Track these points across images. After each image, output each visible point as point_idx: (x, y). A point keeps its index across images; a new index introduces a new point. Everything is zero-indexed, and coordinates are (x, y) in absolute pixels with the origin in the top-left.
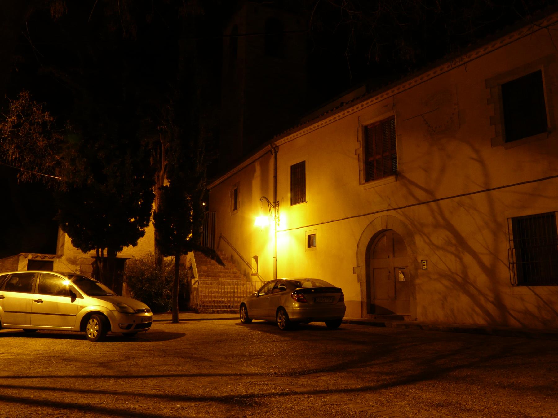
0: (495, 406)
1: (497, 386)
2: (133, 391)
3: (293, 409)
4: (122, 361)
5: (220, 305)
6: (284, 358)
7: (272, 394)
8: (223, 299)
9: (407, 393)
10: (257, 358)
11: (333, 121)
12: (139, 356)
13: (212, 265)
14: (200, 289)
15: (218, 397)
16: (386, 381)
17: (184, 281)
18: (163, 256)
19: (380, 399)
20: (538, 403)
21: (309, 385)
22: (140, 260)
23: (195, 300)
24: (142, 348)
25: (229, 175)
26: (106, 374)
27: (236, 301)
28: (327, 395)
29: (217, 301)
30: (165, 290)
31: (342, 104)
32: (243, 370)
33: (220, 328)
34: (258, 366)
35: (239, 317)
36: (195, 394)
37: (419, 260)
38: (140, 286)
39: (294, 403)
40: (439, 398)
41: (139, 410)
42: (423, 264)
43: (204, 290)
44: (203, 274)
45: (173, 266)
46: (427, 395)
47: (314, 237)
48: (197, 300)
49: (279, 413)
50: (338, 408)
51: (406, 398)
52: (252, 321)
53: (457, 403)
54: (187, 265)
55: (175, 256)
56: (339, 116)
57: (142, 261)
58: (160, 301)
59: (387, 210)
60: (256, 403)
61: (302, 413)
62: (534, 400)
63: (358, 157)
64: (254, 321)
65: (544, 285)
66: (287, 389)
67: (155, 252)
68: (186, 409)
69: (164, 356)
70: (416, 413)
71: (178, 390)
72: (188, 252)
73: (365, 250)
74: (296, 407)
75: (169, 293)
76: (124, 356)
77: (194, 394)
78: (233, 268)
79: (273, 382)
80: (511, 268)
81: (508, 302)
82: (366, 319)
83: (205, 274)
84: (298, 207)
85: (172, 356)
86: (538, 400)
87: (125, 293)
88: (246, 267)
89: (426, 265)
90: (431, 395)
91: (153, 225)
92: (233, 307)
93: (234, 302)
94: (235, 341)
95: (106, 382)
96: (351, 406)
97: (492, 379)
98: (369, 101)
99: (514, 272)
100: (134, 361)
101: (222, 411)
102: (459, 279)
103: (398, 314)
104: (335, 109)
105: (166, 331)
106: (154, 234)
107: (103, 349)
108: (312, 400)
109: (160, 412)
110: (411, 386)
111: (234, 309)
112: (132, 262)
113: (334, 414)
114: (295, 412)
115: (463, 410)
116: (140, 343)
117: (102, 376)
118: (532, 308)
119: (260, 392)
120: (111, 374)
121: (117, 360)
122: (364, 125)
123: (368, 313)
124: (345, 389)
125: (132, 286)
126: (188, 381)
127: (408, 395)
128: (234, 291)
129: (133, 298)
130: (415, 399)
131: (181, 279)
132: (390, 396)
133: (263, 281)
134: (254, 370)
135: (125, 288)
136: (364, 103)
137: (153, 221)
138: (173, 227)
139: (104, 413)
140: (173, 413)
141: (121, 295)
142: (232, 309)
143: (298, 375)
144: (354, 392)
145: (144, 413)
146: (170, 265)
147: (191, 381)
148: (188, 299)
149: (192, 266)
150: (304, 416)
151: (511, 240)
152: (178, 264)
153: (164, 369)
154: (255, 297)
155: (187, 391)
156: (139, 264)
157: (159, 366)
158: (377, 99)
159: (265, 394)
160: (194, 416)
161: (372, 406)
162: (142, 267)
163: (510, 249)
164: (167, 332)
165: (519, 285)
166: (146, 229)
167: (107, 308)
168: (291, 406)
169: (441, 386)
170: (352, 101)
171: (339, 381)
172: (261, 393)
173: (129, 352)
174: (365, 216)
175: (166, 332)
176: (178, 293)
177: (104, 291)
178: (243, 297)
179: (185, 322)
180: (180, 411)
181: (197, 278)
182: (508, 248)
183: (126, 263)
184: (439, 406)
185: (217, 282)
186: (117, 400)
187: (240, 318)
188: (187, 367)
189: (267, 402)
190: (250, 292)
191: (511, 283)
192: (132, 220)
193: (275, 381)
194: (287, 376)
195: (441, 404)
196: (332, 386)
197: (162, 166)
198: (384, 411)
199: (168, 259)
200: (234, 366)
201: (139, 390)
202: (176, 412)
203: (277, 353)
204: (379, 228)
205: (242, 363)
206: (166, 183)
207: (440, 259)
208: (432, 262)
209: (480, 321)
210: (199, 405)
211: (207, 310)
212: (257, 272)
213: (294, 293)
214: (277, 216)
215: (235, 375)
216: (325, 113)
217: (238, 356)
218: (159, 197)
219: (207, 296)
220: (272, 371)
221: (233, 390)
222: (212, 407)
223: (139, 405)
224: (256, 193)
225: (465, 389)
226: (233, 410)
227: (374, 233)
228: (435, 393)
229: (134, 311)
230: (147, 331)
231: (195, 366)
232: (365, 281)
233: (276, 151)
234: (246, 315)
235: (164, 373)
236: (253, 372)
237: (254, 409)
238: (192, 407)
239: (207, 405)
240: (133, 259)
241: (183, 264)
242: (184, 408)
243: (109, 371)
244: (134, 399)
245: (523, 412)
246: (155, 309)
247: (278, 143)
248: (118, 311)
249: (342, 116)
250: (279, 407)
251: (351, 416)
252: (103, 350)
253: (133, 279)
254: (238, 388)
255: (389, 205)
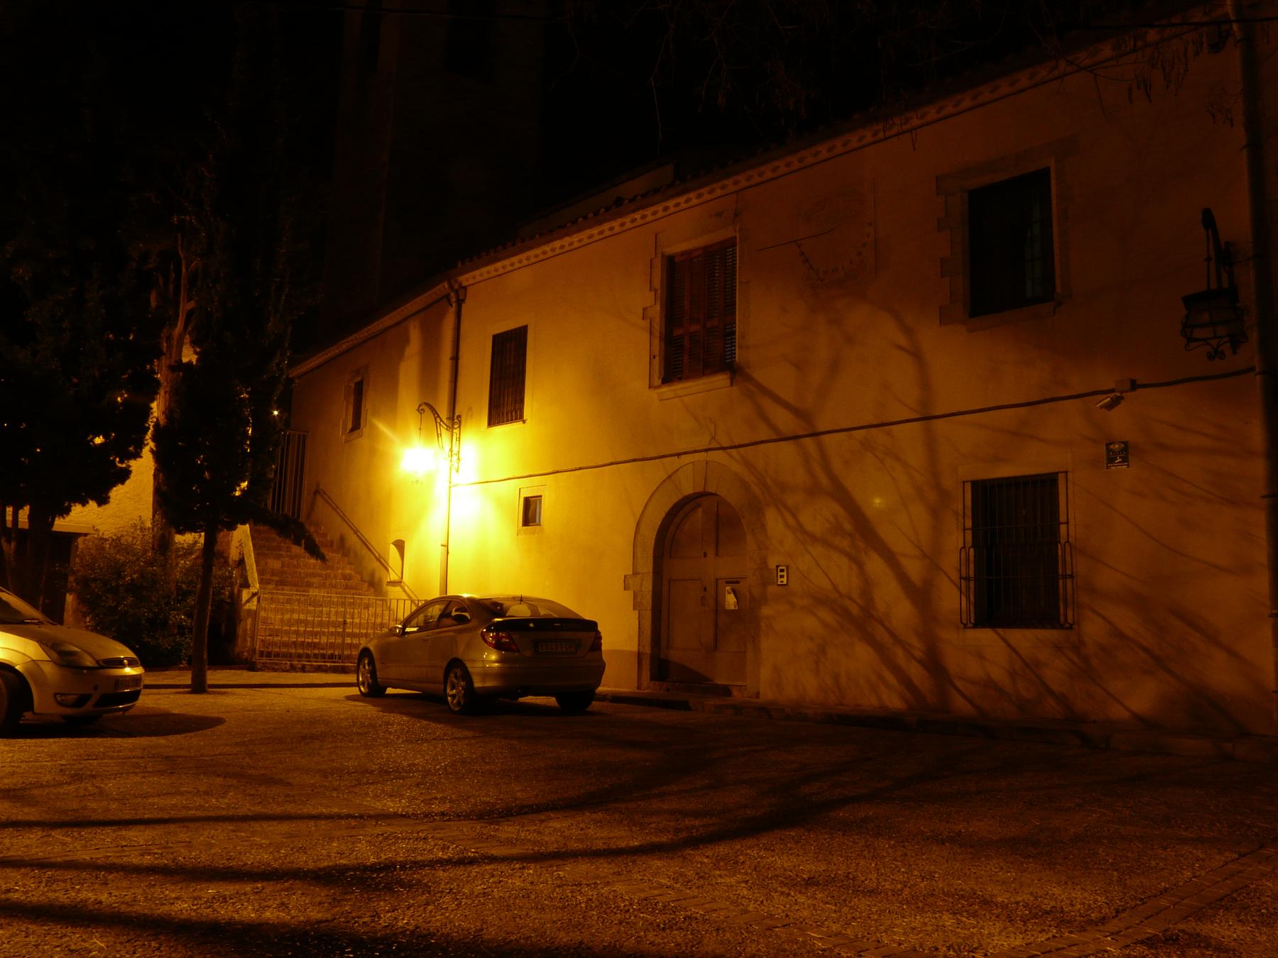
0: (923, 881)
1: (928, 839)
2: (92, 859)
3: (489, 895)
4: (60, 784)
5: (310, 652)
6: (462, 777)
7: (437, 861)
8: (316, 638)
9: (741, 857)
10: (400, 779)
11: (597, 237)
12: (107, 773)
13: (292, 557)
14: (263, 614)
15: (309, 870)
16: (695, 831)
17: (223, 593)
18: (174, 530)
19: (683, 870)
20: (1009, 874)
21: (523, 840)
22: (113, 540)
23: (249, 639)
24: (114, 752)
25: (344, 346)
26: (20, 818)
27: (347, 644)
28: (564, 863)
29: (303, 642)
30: (176, 613)
31: (619, 202)
32: (366, 805)
33: (308, 708)
34: (402, 796)
35: (356, 681)
36: (252, 863)
37: (772, 566)
38: (111, 602)
39: (491, 881)
40: (810, 867)
41: (111, 905)
42: (780, 574)
43: (271, 615)
44: (269, 578)
45: (197, 557)
46: (784, 861)
47: (538, 503)
48: (253, 640)
49: (457, 905)
50: (590, 893)
51: (740, 869)
52: (385, 691)
53: (848, 877)
54: (231, 557)
55: (203, 534)
56: (611, 229)
57: (120, 541)
58: (161, 638)
59: (706, 450)
60: (401, 883)
61: (509, 906)
62: (1002, 868)
63: (649, 326)
64: (390, 691)
65: (1027, 627)
66: (473, 850)
67: (154, 522)
68: (231, 901)
69: (172, 773)
70: (762, 901)
71: (209, 855)
72: (237, 524)
73: (654, 537)
74: (495, 890)
75: (185, 621)
76: (67, 773)
77: (249, 863)
78: (343, 568)
79: (439, 833)
80: (963, 589)
81: (954, 661)
82: (649, 691)
83: (275, 578)
84: (505, 432)
85: (191, 772)
86: (1009, 867)
87: (70, 619)
88: (376, 564)
89: (785, 577)
90: (792, 862)
91: (150, 456)
92: (340, 659)
93: (343, 646)
94: (347, 737)
95: (21, 837)
96: (620, 888)
97: (918, 825)
98: (682, 199)
99: (968, 598)
100: (93, 785)
101: (320, 903)
102: (855, 610)
103: (719, 682)
104: (603, 210)
105: (176, 711)
106: (152, 477)
107: (10, 755)
108: (530, 874)
109: (166, 908)
110: (750, 842)
111: (342, 662)
112: (93, 542)
113: (582, 905)
114: (493, 904)
115: (859, 892)
116: (109, 741)
117: (10, 821)
118: (998, 674)
119: (408, 856)
120: (32, 818)
121: (47, 782)
122: (667, 254)
123: (652, 678)
124: (604, 850)
125: (90, 603)
126: (234, 831)
127: (743, 862)
128: (345, 621)
129: (92, 631)
130: (758, 869)
131: (215, 588)
132: (704, 863)
133: (414, 598)
134: (392, 806)
135: (70, 607)
136: (671, 203)
137: (152, 444)
138: (202, 462)
139: (17, 916)
140: (198, 911)
141: (61, 622)
142: (338, 663)
143: (496, 818)
144: (625, 856)
145: (123, 913)
146: (191, 554)
147: (241, 832)
148: (231, 636)
149: (246, 559)
150: (516, 912)
151: (1064, 523)
152: (212, 553)
153: (173, 802)
154: (396, 635)
155: (231, 856)
156: (110, 548)
157: (159, 796)
158: (711, 192)
159: (421, 861)
160: (253, 915)
161: (667, 887)
162: (118, 556)
163: (964, 547)
164: (178, 714)
165: (975, 626)
166: (134, 464)
167: (24, 654)
168: (484, 889)
169: (814, 841)
170: (644, 196)
171: (590, 831)
172: (413, 859)
173: (80, 763)
174: (657, 461)
175: (174, 715)
176: (208, 621)
177: (17, 612)
178: (366, 635)
179: (223, 690)
180: (216, 905)
181: (255, 587)
182: (961, 545)
183: (77, 545)
184: (810, 885)
185: (303, 598)
186: (51, 881)
187: (357, 685)
188: (229, 800)
189: (426, 881)
190: (382, 625)
191: (961, 621)
192: (99, 440)
193: (443, 831)
194: (472, 819)
195: (815, 880)
196: (576, 843)
197: (181, 314)
198: (694, 897)
199: (184, 539)
200: (345, 796)
201: (108, 857)
202: (205, 908)
203: (446, 766)
204: (688, 490)
205: (364, 790)
206: (189, 356)
207: (818, 564)
208: (799, 569)
209: (894, 701)
210: (263, 888)
211: (277, 664)
212: (402, 578)
213: (489, 630)
214: (455, 449)
215: (348, 817)
216: (581, 219)
217: (353, 773)
218: (168, 389)
219: (278, 630)
220: (435, 808)
221: (344, 854)
222: (294, 894)
223: (110, 893)
224: (408, 395)
225: (862, 847)
226: (346, 900)
227: (674, 500)
228: (801, 857)
229: (97, 662)
230: (127, 710)
231: (250, 795)
232: (650, 607)
233: (460, 298)
234: (371, 677)
235: (173, 814)
236: (391, 810)
237: (397, 898)
238: (245, 894)
239: (283, 890)
240: (96, 536)
241: (223, 552)
242: (226, 898)
243: (26, 810)
244: (97, 878)
245: (980, 893)
246: (150, 660)
247: (465, 279)
248: (55, 663)
249: (617, 229)
250: (455, 893)
251: (621, 911)
252: (9, 757)
253: (93, 585)
254: (356, 847)
255: (713, 438)
